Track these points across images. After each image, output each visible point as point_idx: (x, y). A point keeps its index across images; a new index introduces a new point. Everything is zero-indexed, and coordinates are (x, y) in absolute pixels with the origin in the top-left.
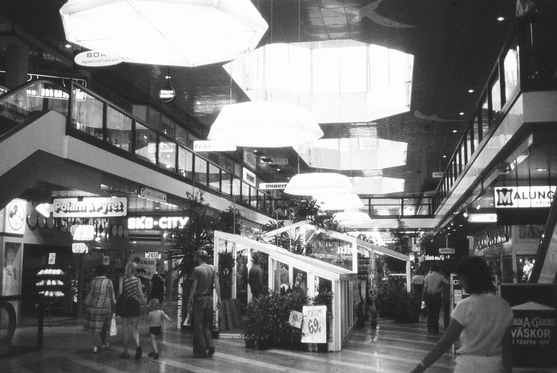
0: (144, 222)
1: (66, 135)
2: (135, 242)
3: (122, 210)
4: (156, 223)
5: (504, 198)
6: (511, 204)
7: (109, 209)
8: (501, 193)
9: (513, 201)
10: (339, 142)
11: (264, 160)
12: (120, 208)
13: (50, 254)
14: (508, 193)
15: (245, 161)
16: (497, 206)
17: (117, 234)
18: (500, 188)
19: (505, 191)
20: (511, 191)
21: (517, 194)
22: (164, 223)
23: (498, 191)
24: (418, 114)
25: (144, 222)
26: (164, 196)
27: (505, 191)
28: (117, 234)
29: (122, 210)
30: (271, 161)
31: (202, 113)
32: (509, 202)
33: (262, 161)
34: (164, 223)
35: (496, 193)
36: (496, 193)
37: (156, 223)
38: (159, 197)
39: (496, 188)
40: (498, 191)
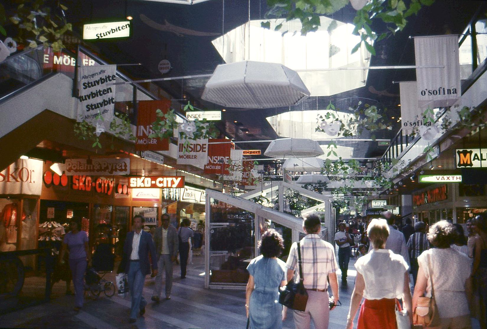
0: (143, 182)
1: (73, 97)
2: (13, 217)
3: (126, 170)
4: (153, 182)
5: (465, 159)
6: (471, 164)
7: (114, 168)
8: (462, 155)
9: (473, 162)
10: (302, 114)
11: (242, 130)
12: (123, 168)
13: (54, 209)
14: (468, 155)
15: (227, 130)
16: (458, 167)
17: (52, 182)
18: (461, 150)
19: (465, 153)
20: (471, 152)
21: (476, 155)
22: (160, 182)
23: (459, 153)
24: (372, 89)
25: (143, 182)
26: (162, 158)
27: (465, 153)
28: (52, 182)
29: (126, 170)
30: (248, 131)
31: (193, 87)
32: (469, 163)
33: (241, 131)
34: (160, 182)
35: (457, 155)
36: (457, 155)
37: (153, 182)
38: (157, 158)
39: (457, 150)
40: (459, 153)
